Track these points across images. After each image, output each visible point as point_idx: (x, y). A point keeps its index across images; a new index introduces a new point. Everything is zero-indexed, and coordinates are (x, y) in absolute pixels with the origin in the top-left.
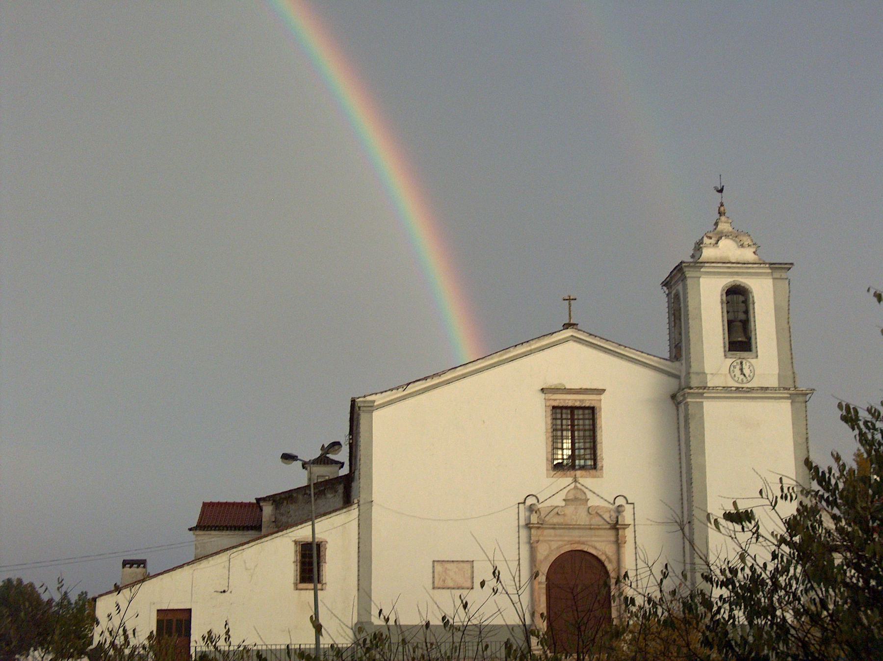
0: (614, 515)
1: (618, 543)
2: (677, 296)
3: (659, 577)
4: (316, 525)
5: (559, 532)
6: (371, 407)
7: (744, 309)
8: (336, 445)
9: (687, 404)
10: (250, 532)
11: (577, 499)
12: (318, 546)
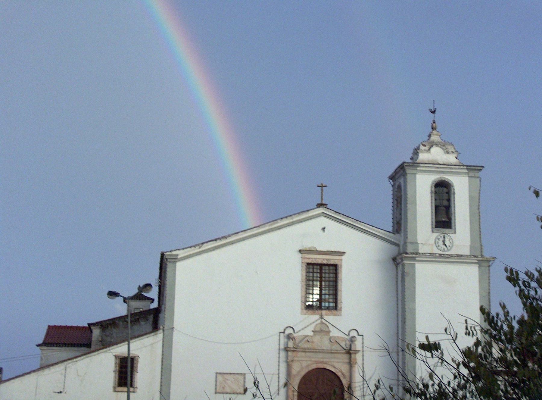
0: (348, 343)
1: (351, 364)
2: (399, 187)
3: (373, 388)
4: (131, 345)
5: (308, 354)
6: (176, 259)
7: (447, 198)
8: (148, 286)
9: (403, 265)
10: (83, 348)
11: (322, 330)
12: (133, 359)
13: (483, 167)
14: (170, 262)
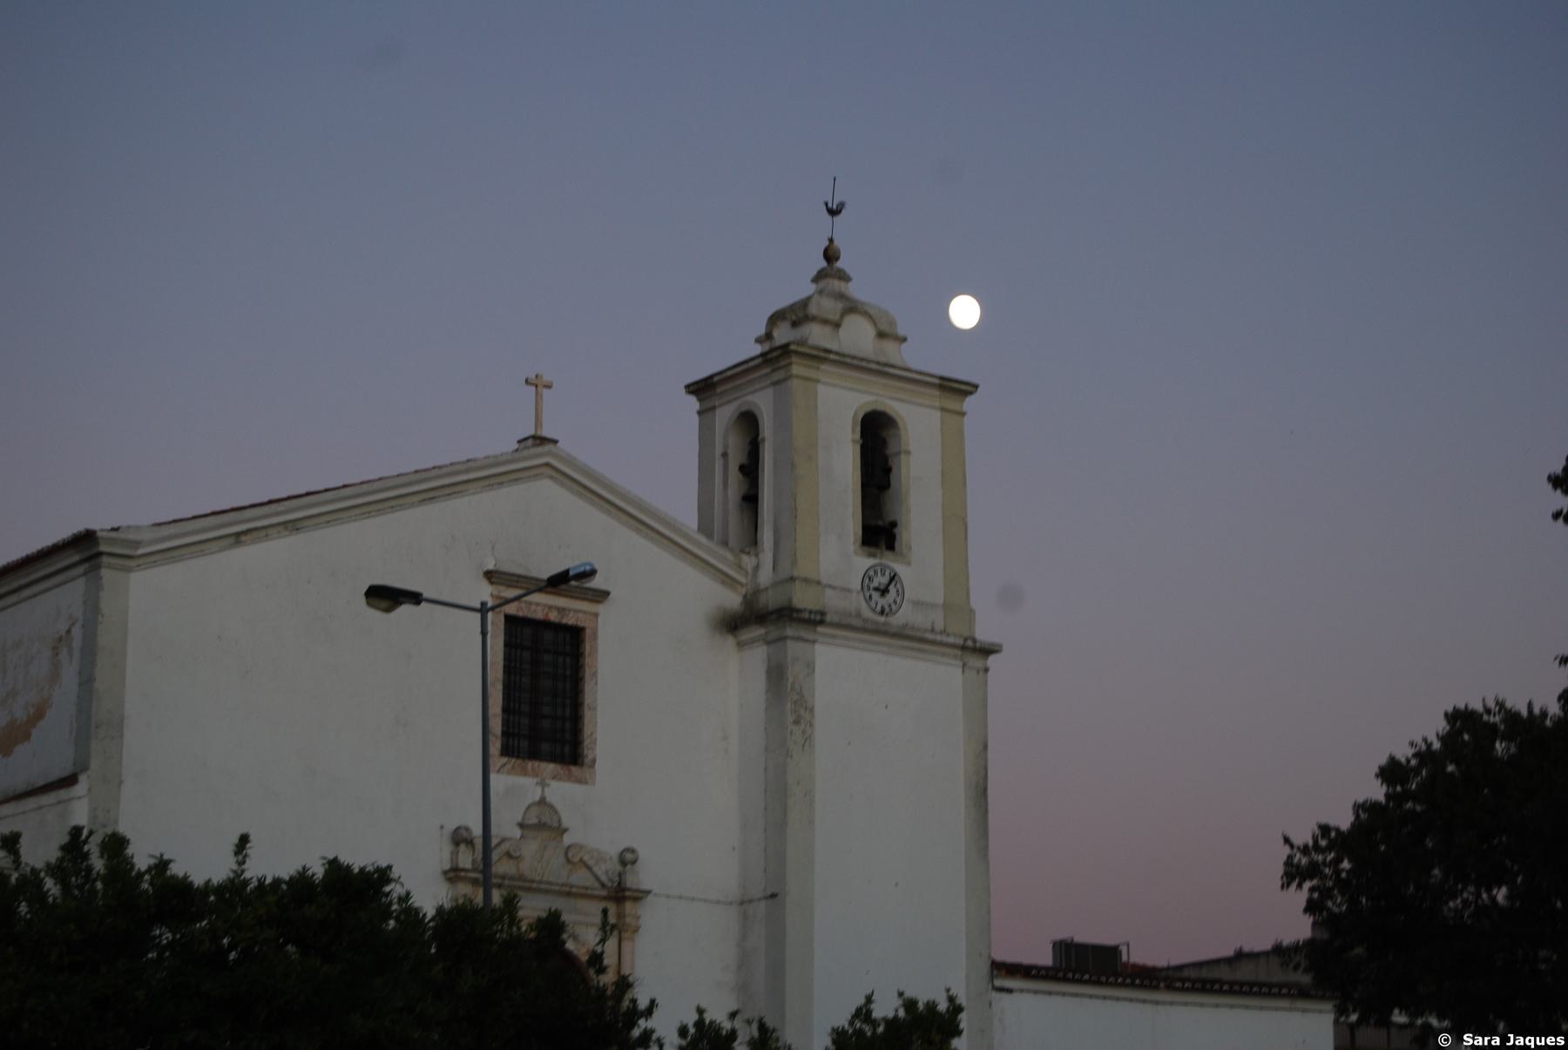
13: (976, 387)
14: (109, 567)
